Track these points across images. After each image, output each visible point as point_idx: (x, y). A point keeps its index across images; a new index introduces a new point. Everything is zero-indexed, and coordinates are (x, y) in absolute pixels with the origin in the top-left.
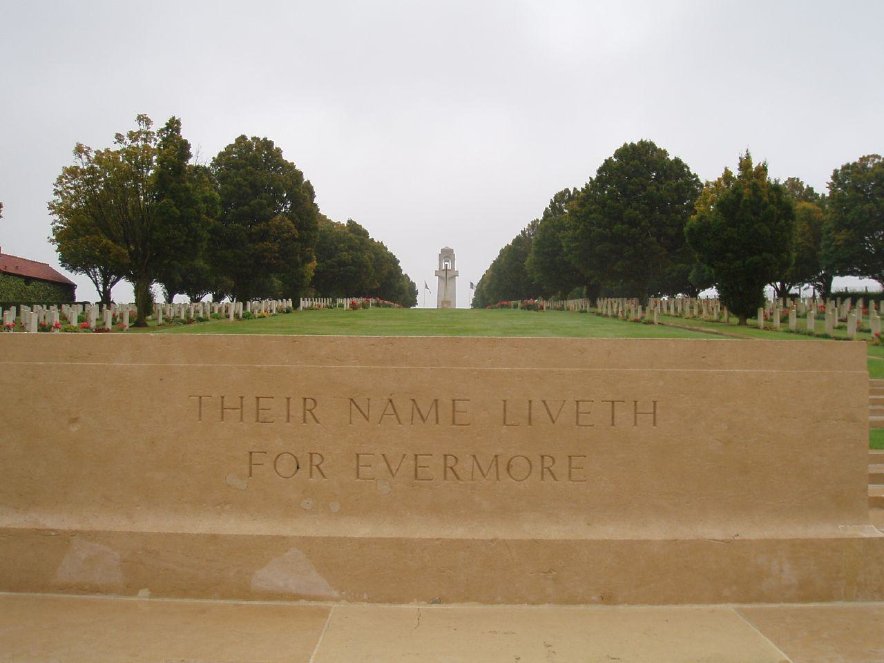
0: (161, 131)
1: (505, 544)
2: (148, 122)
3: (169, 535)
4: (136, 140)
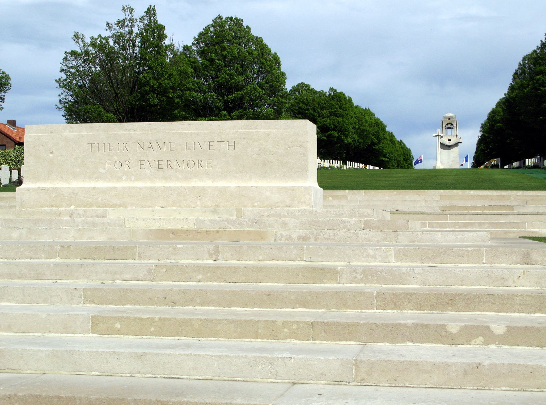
0: (142, 18)
1: (184, 188)
2: (132, 10)
3: (81, 188)
4: (123, 26)
